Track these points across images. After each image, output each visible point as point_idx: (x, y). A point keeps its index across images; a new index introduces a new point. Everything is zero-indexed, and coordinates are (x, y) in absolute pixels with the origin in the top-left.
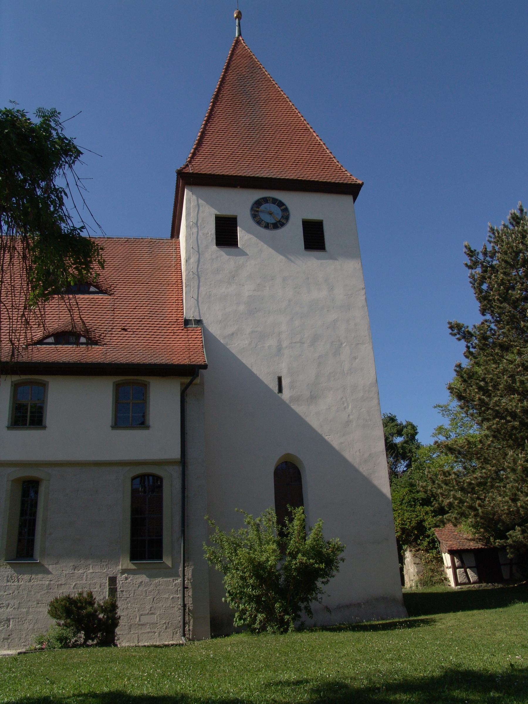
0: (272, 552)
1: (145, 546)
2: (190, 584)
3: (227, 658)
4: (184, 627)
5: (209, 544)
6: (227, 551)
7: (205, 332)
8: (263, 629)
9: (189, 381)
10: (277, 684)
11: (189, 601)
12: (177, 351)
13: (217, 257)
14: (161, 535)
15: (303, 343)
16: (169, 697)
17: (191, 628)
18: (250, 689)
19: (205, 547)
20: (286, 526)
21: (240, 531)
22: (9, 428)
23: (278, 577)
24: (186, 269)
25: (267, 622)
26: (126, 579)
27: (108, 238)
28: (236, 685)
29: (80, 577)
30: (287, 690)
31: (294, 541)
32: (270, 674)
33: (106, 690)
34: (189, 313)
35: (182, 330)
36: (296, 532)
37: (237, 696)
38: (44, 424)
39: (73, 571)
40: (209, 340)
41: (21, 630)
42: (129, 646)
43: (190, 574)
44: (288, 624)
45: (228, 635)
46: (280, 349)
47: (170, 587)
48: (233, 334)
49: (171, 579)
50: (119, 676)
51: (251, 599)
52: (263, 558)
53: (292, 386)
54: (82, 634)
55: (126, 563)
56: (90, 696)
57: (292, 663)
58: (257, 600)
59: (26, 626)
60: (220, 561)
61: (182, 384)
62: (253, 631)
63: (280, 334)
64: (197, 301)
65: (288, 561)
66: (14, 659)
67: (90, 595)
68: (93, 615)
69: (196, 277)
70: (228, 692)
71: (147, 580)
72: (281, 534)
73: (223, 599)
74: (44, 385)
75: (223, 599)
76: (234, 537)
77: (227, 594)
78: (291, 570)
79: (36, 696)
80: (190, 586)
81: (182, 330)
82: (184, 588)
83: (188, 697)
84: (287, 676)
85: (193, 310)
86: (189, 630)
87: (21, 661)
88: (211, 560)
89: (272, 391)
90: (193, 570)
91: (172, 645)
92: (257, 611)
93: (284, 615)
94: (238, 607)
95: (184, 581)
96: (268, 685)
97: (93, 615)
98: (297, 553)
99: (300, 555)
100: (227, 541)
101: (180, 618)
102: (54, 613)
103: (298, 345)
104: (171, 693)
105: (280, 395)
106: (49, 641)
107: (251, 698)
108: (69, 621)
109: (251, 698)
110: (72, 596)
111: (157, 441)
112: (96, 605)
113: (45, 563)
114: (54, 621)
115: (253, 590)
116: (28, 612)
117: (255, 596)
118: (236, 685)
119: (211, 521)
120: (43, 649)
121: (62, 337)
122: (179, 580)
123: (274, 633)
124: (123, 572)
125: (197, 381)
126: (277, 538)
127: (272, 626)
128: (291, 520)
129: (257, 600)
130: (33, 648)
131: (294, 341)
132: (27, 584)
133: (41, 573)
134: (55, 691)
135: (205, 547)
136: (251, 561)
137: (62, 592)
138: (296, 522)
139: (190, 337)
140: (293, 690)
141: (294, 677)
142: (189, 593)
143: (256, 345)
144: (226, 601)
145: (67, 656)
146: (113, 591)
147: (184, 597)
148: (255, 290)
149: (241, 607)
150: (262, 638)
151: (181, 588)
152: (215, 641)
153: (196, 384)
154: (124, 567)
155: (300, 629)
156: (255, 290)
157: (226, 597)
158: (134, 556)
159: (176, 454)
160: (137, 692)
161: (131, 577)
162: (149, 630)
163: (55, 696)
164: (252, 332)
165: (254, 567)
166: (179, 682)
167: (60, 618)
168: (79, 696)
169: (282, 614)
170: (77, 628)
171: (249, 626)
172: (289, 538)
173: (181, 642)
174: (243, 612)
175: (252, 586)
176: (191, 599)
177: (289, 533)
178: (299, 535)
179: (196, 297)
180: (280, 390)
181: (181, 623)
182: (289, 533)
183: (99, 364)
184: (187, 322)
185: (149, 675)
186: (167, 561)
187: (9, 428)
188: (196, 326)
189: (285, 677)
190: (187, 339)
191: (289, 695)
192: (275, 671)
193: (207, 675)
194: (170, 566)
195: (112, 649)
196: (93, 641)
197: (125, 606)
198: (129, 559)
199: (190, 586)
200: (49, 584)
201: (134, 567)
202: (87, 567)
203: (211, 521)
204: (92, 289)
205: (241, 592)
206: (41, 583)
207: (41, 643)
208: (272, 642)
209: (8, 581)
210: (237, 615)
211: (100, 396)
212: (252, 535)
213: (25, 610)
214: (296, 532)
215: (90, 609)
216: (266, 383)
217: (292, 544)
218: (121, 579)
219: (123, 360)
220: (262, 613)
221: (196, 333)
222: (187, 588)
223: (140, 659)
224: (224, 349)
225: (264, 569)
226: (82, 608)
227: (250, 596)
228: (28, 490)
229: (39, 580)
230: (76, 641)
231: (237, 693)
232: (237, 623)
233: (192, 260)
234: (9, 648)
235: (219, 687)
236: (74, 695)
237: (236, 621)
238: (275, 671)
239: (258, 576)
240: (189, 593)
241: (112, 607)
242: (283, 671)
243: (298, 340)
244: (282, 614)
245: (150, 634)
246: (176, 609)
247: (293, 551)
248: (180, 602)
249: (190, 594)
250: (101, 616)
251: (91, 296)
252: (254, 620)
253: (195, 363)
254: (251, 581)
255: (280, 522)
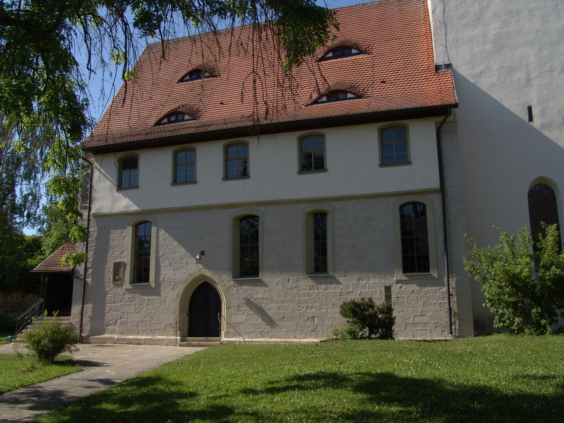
0: (526, 265)
1: (415, 260)
2: (454, 292)
3: (484, 353)
4: (451, 327)
5: (468, 259)
6: (484, 264)
7: (455, 75)
8: (521, 330)
9: (442, 119)
10: (524, 377)
11: (454, 306)
12: (431, 94)
13: (461, 3)
14: (427, 252)
15: (553, 71)
16: (428, 380)
17: (457, 327)
18: (499, 379)
19: (465, 261)
20: (539, 241)
21: (496, 247)
22: (299, 173)
23: (534, 286)
24: (434, 20)
25: (524, 325)
26: (401, 287)
27: (363, 5)
28: (487, 375)
29: (364, 287)
30: (533, 382)
31: (548, 255)
32: (519, 368)
33: (379, 371)
34: (439, 60)
35: (434, 75)
36: (549, 247)
37: (486, 384)
38: (325, 167)
39: (358, 282)
40: (458, 80)
41: (323, 325)
42: (405, 340)
43: (454, 284)
44: (544, 327)
45: (489, 334)
46: (528, 81)
47: (437, 295)
48: (481, 73)
49: (438, 288)
50: (391, 362)
51: (508, 305)
52: (518, 270)
53: (542, 113)
54: (367, 329)
55: (399, 275)
56: (367, 375)
57: (542, 361)
58: (514, 305)
59: (326, 322)
60: (479, 273)
61: (436, 123)
62: (512, 332)
63: (528, 66)
64: (446, 47)
65: (542, 273)
66: (317, 345)
67: (370, 300)
68: (374, 316)
69: (443, 25)
70: (479, 380)
71: (418, 288)
72: (535, 249)
73: (484, 305)
74: (322, 136)
75: (484, 305)
76: (490, 252)
77: (487, 301)
78: (545, 280)
79: (328, 372)
80: (454, 294)
81: (434, 75)
82: (449, 295)
83: (444, 382)
84: (534, 371)
85: (442, 56)
86: (455, 329)
87: (321, 347)
88: (471, 272)
89: (522, 120)
90: (456, 281)
91: (439, 340)
92: (515, 315)
93: (540, 320)
94: (497, 311)
95: (449, 289)
96: (516, 377)
97: (374, 316)
98: (551, 266)
99: (553, 268)
100: (484, 256)
101: (448, 319)
102: (344, 313)
103: (548, 73)
104: (431, 377)
105: (530, 123)
106: (342, 334)
107: (498, 387)
108: (355, 319)
109: (498, 387)
110: (356, 301)
111: (419, 174)
112: (376, 308)
113: (337, 276)
114: (344, 320)
115: (509, 297)
116: (327, 312)
117: (512, 303)
118: (487, 375)
119: (470, 239)
120: (338, 339)
121: (175, 115)
122: (445, 289)
123: (531, 334)
124: (398, 282)
125: (451, 118)
126: (531, 252)
127: (529, 329)
128: (544, 236)
129: (514, 305)
130: (331, 338)
131: (544, 70)
132: (325, 291)
133: (331, 283)
134: (342, 369)
135: (465, 261)
136: (506, 272)
137: (349, 298)
138: (550, 238)
139: (441, 80)
140: (539, 384)
141: (541, 372)
142: (454, 299)
143: (505, 80)
144: (486, 306)
145: (354, 346)
146: (388, 297)
147: (449, 302)
148: (501, 28)
149: (500, 311)
150: (519, 338)
151: (447, 295)
152: (477, 338)
153: (449, 122)
154: (398, 279)
155: (556, 332)
156: (501, 28)
157: (486, 303)
158: (406, 269)
159: (436, 184)
160: (404, 375)
161: (405, 286)
162: (422, 328)
163: (341, 373)
164: (500, 68)
165: (509, 277)
166: (439, 369)
167: (349, 317)
168: (358, 374)
169: (538, 318)
170: (362, 325)
171: (508, 327)
172: (543, 252)
173: (448, 338)
174: (502, 315)
175: (509, 294)
176: (456, 304)
177: (542, 248)
178: (553, 249)
179: (444, 44)
180: (531, 118)
181: (448, 323)
182: (542, 248)
183: (364, 114)
184: (437, 68)
185: (415, 362)
186: (434, 273)
187: (299, 173)
188: (446, 70)
189: (533, 372)
190: (439, 83)
191: (535, 388)
192: (524, 366)
193: (464, 365)
194: (437, 277)
195: (390, 342)
196: (376, 335)
197: (401, 309)
198: (401, 272)
199: (454, 294)
200: (341, 292)
201: (406, 278)
202: (369, 278)
203: (470, 239)
204: (354, 51)
205: (498, 299)
206: (334, 291)
207: (337, 335)
208: (528, 341)
209: (310, 290)
210: (496, 318)
211: (368, 139)
212: (507, 250)
213: (324, 311)
214: (549, 247)
215: (371, 311)
216: (516, 113)
217: (545, 258)
218: (395, 289)
219: (384, 109)
220: (518, 317)
221: (446, 77)
222: (452, 295)
223: (410, 350)
224: (474, 87)
225: (519, 279)
226: (364, 310)
227: (506, 302)
228: (319, 221)
229: (333, 289)
230: (363, 334)
231: (487, 382)
232: (497, 325)
233: (438, 10)
234: (316, 338)
235: (472, 376)
236: (355, 373)
237: (496, 323)
238: (524, 366)
239: (513, 286)
240: (454, 299)
241: (389, 310)
242: (532, 367)
243: (548, 69)
244: (538, 318)
245: (423, 331)
246: (443, 312)
247: (546, 264)
248: (447, 306)
249: (455, 300)
250: (380, 316)
251: (353, 57)
252: (512, 323)
253: (446, 103)
254: (508, 290)
255: (535, 238)
